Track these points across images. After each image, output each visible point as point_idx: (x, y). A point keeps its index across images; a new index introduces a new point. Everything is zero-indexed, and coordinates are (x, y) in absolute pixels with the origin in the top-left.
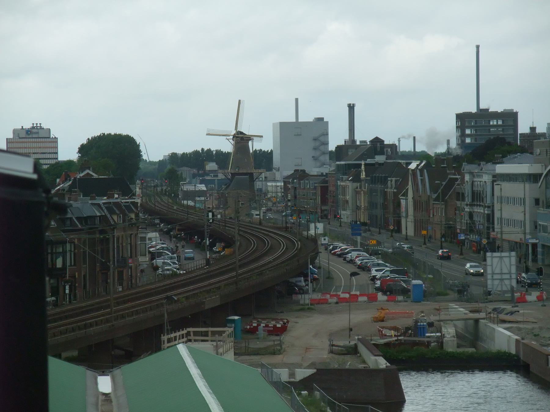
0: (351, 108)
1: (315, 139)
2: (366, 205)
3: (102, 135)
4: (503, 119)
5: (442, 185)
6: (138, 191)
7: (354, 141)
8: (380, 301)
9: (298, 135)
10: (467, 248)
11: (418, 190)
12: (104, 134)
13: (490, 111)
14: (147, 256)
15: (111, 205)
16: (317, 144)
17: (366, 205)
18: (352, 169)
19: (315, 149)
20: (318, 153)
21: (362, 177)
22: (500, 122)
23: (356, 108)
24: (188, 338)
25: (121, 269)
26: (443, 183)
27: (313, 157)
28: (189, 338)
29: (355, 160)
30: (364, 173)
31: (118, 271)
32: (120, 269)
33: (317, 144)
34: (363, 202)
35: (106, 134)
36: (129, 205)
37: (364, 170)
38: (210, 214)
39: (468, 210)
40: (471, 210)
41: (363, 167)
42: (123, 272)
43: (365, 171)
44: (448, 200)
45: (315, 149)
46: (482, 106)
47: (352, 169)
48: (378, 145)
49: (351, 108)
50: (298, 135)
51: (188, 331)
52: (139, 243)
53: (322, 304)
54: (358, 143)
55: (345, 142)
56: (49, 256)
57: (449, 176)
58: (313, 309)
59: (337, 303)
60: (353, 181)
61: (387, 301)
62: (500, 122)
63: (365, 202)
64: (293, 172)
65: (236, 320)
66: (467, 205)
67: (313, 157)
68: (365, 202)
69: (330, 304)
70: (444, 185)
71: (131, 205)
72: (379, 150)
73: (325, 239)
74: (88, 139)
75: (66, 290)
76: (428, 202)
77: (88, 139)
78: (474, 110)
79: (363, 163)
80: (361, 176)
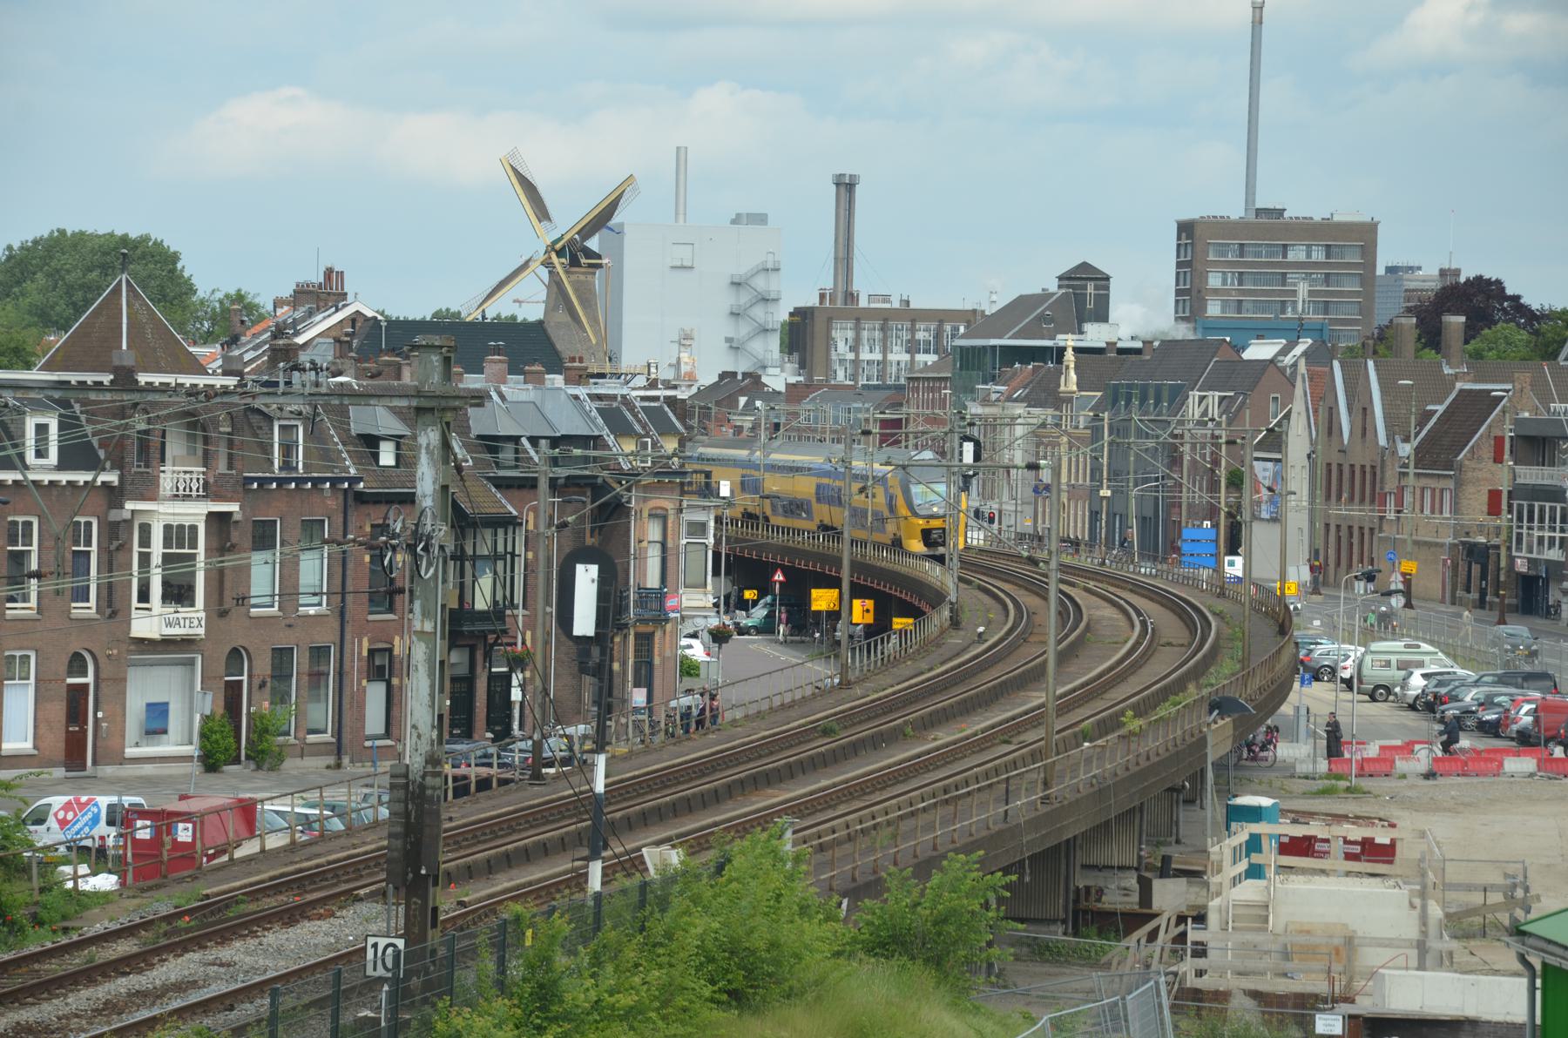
0: (846, 186)
1: (736, 284)
2: (1085, 480)
3: (56, 234)
6: (686, 360)
7: (851, 297)
11: (1332, 427)
12: (62, 232)
14: (709, 587)
15: (615, 405)
17: (1085, 480)
18: (1017, 365)
21: (1062, 388)
22: (1318, 255)
23: (859, 191)
24: (1252, 861)
25: (649, 629)
27: (728, 340)
28: (1256, 858)
29: (1013, 337)
30: (1073, 376)
31: (637, 635)
32: (642, 629)
33: (745, 298)
34: (1069, 468)
35: (69, 233)
36: (618, 408)
37: (1072, 365)
38: (969, 448)
41: (1069, 356)
42: (653, 640)
43: (1076, 368)
44: (1467, 462)
47: (1017, 365)
49: (846, 186)
51: (1251, 835)
52: (684, 541)
53: (1371, 776)
56: (277, 592)
57: (1459, 385)
59: (1429, 775)
60: (1031, 401)
62: (1318, 255)
63: (1073, 470)
64: (716, 379)
65: (1266, 808)
67: (728, 340)
68: (1073, 470)
69: (1404, 776)
70: (1437, 415)
71: (667, 409)
73: (1232, 564)
74: (10, 248)
75: (513, 690)
76: (1378, 472)
77: (10, 248)
78: (1234, 209)
79: (1069, 341)
80: (1059, 386)
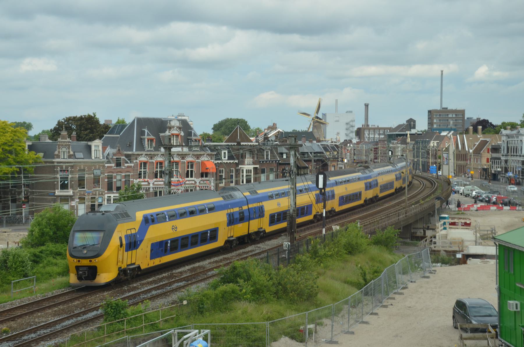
1: (347, 124)
4: (457, 114)
5: (475, 145)
7: (368, 125)
8: (505, 210)
9: (337, 121)
10: (502, 182)
12: (228, 119)
13: (448, 109)
16: (348, 126)
19: (347, 129)
20: (348, 132)
22: (454, 116)
26: (476, 143)
27: (346, 134)
28: (445, 226)
30: (409, 139)
33: (348, 126)
39: (504, 159)
40: (506, 159)
45: (347, 129)
46: (444, 106)
48: (412, 123)
49: (367, 106)
50: (337, 121)
54: (370, 127)
55: (363, 126)
58: (466, 214)
60: (401, 144)
61: (510, 210)
66: (503, 155)
72: (412, 126)
77: (219, 122)
78: (438, 108)
79: (408, 132)
